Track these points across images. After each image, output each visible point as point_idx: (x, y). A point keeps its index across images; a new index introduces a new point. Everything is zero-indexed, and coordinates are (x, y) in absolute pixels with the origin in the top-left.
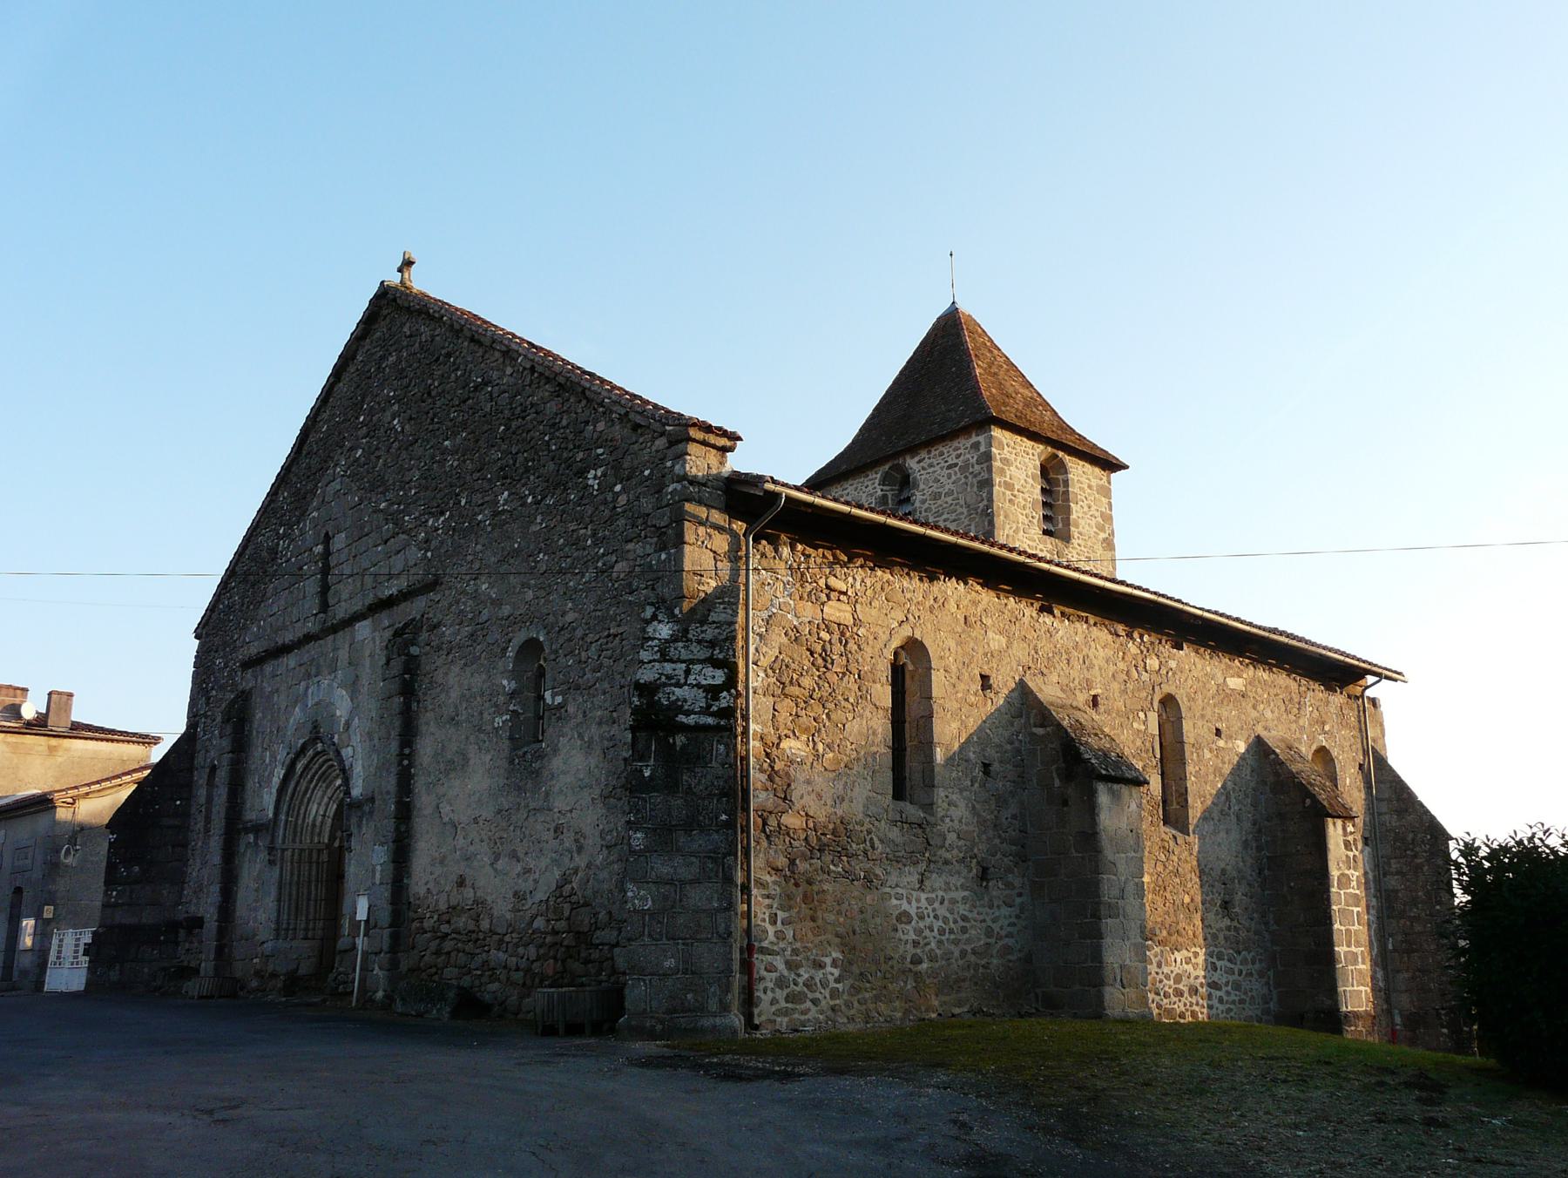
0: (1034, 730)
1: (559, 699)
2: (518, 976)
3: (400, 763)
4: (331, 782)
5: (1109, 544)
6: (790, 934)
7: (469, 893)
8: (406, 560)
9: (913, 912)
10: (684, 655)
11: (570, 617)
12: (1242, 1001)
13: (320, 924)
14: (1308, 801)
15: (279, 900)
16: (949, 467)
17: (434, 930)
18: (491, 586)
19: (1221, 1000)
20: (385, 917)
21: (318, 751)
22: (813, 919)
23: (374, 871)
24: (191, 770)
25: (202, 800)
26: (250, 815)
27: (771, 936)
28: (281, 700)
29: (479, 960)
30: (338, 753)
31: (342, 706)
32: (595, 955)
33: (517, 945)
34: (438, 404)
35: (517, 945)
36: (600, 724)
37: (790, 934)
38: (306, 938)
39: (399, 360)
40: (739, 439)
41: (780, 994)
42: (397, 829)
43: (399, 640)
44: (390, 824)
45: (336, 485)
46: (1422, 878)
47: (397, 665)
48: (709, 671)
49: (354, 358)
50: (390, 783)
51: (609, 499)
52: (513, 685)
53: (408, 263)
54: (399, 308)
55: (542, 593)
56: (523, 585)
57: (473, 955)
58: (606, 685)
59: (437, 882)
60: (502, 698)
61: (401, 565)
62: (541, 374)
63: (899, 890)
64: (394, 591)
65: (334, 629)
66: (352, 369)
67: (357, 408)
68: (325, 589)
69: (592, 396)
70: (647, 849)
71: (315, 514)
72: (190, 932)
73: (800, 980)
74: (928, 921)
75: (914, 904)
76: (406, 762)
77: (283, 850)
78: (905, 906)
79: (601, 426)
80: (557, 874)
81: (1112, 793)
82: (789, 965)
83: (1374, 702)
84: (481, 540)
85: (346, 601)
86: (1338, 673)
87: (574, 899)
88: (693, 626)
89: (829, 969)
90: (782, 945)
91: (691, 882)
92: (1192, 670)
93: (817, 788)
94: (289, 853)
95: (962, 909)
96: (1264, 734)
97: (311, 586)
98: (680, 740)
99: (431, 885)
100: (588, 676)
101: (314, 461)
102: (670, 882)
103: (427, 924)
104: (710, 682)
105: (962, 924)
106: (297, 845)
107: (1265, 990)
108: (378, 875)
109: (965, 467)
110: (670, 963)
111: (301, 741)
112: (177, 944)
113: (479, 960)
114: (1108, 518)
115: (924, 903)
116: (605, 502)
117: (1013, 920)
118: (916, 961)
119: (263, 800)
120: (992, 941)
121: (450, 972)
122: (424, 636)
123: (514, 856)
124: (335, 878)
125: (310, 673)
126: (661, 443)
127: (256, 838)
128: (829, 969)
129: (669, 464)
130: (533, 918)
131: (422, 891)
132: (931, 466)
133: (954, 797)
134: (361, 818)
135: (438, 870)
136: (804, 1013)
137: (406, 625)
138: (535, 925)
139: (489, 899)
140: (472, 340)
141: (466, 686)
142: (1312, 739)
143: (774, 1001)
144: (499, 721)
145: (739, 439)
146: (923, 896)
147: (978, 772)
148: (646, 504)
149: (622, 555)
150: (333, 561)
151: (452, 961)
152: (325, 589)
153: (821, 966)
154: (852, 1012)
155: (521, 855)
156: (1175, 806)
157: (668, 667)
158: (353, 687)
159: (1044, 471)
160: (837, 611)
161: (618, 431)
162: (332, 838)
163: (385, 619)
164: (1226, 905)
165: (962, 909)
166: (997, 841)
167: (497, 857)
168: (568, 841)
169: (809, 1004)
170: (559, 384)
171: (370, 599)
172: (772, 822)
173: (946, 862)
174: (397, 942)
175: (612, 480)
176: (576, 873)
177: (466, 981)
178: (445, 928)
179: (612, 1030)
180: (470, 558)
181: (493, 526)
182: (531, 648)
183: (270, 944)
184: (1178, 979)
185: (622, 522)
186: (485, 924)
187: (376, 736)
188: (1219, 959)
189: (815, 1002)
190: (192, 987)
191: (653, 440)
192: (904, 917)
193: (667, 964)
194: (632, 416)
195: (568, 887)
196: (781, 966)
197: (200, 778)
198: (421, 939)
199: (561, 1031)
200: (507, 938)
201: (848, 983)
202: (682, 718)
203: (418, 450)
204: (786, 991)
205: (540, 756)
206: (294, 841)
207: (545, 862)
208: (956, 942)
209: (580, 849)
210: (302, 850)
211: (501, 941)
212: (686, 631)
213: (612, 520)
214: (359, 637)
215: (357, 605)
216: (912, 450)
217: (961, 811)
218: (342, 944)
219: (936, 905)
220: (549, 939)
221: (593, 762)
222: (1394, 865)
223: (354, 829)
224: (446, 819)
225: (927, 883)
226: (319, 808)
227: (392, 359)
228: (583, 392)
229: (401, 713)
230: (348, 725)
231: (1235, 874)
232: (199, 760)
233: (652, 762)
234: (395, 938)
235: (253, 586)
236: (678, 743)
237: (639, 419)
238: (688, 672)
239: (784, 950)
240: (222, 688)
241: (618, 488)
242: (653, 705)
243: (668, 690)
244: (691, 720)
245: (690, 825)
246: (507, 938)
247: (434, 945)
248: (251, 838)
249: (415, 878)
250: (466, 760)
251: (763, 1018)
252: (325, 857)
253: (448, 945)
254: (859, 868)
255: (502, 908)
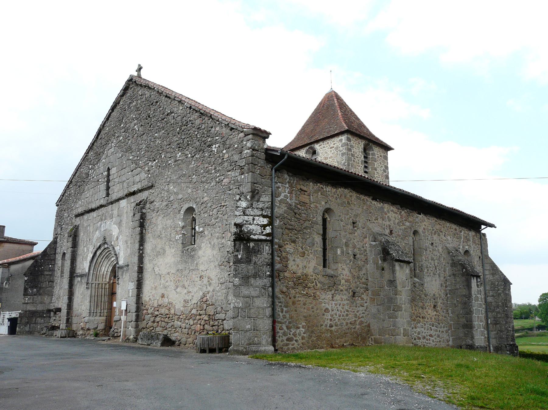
0: (371, 243)
1: (201, 229)
2: (186, 331)
3: (139, 253)
4: (110, 259)
5: (387, 177)
6: (288, 316)
7: (166, 300)
8: (140, 177)
9: (330, 309)
10: (252, 213)
11: (206, 199)
12: (440, 341)
13: (106, 311)
14: (464, 270)
15: (90, 302)
16: (331, 148)
17: (152, 314)
18: (174, 187)
19: (433, 341)
20: (133, 308)
21: (104, 249)
22: (296, 311)
23: (129, 292)
24: (55, 254)
25: (60, 265)
26: (79, 271)
27: (281, 317)
28: (91, 229)
29: (170, 325)
30: (114, 248)
31: (115, 231)
32: (216, 323)
33: (185, 319)
34: (153, 120)
35: (185, 319)
36: (218, 238)
37: (288, 316)
38: (100, 316)
39: (137, 104)
40: (270, 134)
41: (285, 338)
42: (138, 276)
43: (138, 207)
44: (136, 274)
45: (112, 150)
46: (500, 298)
47: (138, 216)
48: (261, 219)
49: (119, 103)
50: (136, 259)
51: (221, 155)
52: (183, 224)
53: (140, 69)
54: (137, 85)
55: (195, 190)
56: (187, 187)
57: (167, 323)
58: (220, 224)
59: (153, 296)
60: (179, 229)
61: (140, 179)
62: (194, 109)
63: (325, 300)
64: (136, 189)
65: (112, 203)
66: (118, 107)
67: (121, 121)
68: (108, 188)
69: (215, 118)
70: (240, 285)
71: (104, 160)
72: (55, 313)
73: (291, 333)
74: (335, 312)
75: (330, 305)
76: (141, 252)
77: (92, 284)
78: (327, 306)
79: (217, 129)
80: (201, 294)
81: (400, 266)
82: (288, 328)
83: (484, 235)
84: (170, 171)
85: (117, 192)
86: (473, 224)
87: (208, 303)
88: (254, 203)
89: (301, 329)
90: (285, 320)
91: (256, 297)
92: (425, 223)
93: (297, 263)
94: (94, 285)
95: (346, 307)
96: (448, 245)
97: (103, 187)
98: (252, 244)
99: (151, 297)
100: (213, 221)
101: (103, 142)
102: (248, 297)
103: (150, 311)
104: (263, 223)
105: (346, 313)
106: (97, 282)
107: (448, 338)
108: (130, 294)
109: (337, 148)
110: (248, 327)
111: (99, 244)
112: (50, 317)
113: (170, 325)
114: (387, 168)
115: (334, 305)
116: (219, 157)
117: (364, 311)
118: (331, 326)
119: (83, 266)
120: (357, 319)
121: (158, 329)
122: (148, 206)
123: (184, 286)
124: (112, 294)
125: (102, 219)
126: (242, 135)
127: (81, 280)
128: (301, 329)
129: (245, 143)
130: (192, 310)
131: (147, 299)
132: (324, 147)
133: (344, 267)
134: (123, 272)
135: (154, 292)
136: (293, 345)
137: (141, 202)
138: (192, 312)
139: (174, 302)
140: (166, 96)
141: (165, 225)
142: (463, 247)
143: (282, 341)
144: (177, 237)
145: (270, 134)
146: (333, 303)
147: (352, 257)
148: (236, 157)
149: (226, 177)
150: (111, 178)
151: (160, 325)
152: (108, 188)
153: (298, 328)
154: (309, 344)
155: (187, 287)
156: (418, 271)
157: (246, 218)
158: (120, 224)
159: (365, 150)
160: (304, 198)
161: (225, 131)
162: (110, 279)
163: (132, 199)
164: (435, 306)
165: (346, 307)
166: (358, 283)
167: (177, 287)
168: (205, 280)
169: (294, 342)
170: (201, 113)
171: (126, 192)
172: (282, 275)
173: (342, 291)
174: (138, 318)
175: (222, 149)
176: (208, 293)
177: (165, 332)
178: (157, 313)
179: (227, 351)
180: (166, 177)
181: (175, 166)
182: (190, 210)
183: (87, 318)
184: (419, 333)
185: (226, 164)
186: (172, 311)
187: (129, 242)
188: (433, 326)
189: (296, 341)
190: (58, 333)
191: (238, 134)
192: (327, 310)
193: (247, 327)
194: (230, 125)
195: (205, 298)
196: (285, 328)
197: (59, 257)
198: (147, 317)
199: (207, 351)
200: (181, 317)
201: (308, 334)
202: (252, 236)
203: (144, 137)
204: (287, 337)
205: (193, 250)
206: (96, 280)
207: (196, 289)
208: (344, 320)
209: (210, 284)
210: (99, 284)
211: (179, 318)
212: (252, 204)
213: (222, 163)
214: (122, 206)
215: (121, 194)
216: (317, 142)
217: (346, 272)
218: (116, 318)
219: (338, 306)
220: (198, 317)
221: (215, 252)
222: (491, 293)
223: (120, 276)
224: (157, 273)
225: (335, 298)
226: (106, 269)
227: (134, 104)
228: (211, 116)
229: (140, 234)
230: (117, 238)
231: (438, 296)
232: (58, 250)
233: (241, 253)
234: (137, 316)
235: (79, 187)
236: (251, 246)
237: (233, 126)
238: (254, 219)
239: (286, 322)
240: (67, 224)
241: (224, 151)
242: (241, 231)
243: (247, 226)
244: (256, 237)
245: (255, 276)
246: (181, 317)
247: (152, 319)
248: (79, 279)
249: (144, 295)
250: (165, 251)
251: (279, 347)
252: (107, 286)
253: (158, 319)
254: (311, 292)
255: (179, 306)
